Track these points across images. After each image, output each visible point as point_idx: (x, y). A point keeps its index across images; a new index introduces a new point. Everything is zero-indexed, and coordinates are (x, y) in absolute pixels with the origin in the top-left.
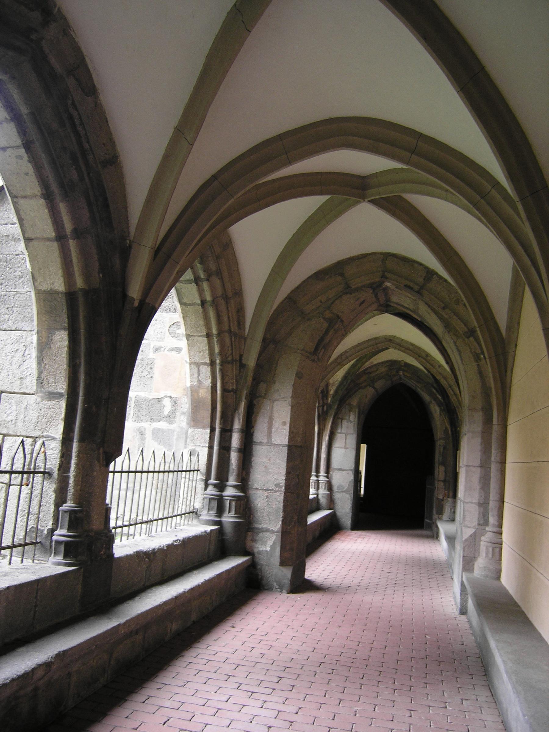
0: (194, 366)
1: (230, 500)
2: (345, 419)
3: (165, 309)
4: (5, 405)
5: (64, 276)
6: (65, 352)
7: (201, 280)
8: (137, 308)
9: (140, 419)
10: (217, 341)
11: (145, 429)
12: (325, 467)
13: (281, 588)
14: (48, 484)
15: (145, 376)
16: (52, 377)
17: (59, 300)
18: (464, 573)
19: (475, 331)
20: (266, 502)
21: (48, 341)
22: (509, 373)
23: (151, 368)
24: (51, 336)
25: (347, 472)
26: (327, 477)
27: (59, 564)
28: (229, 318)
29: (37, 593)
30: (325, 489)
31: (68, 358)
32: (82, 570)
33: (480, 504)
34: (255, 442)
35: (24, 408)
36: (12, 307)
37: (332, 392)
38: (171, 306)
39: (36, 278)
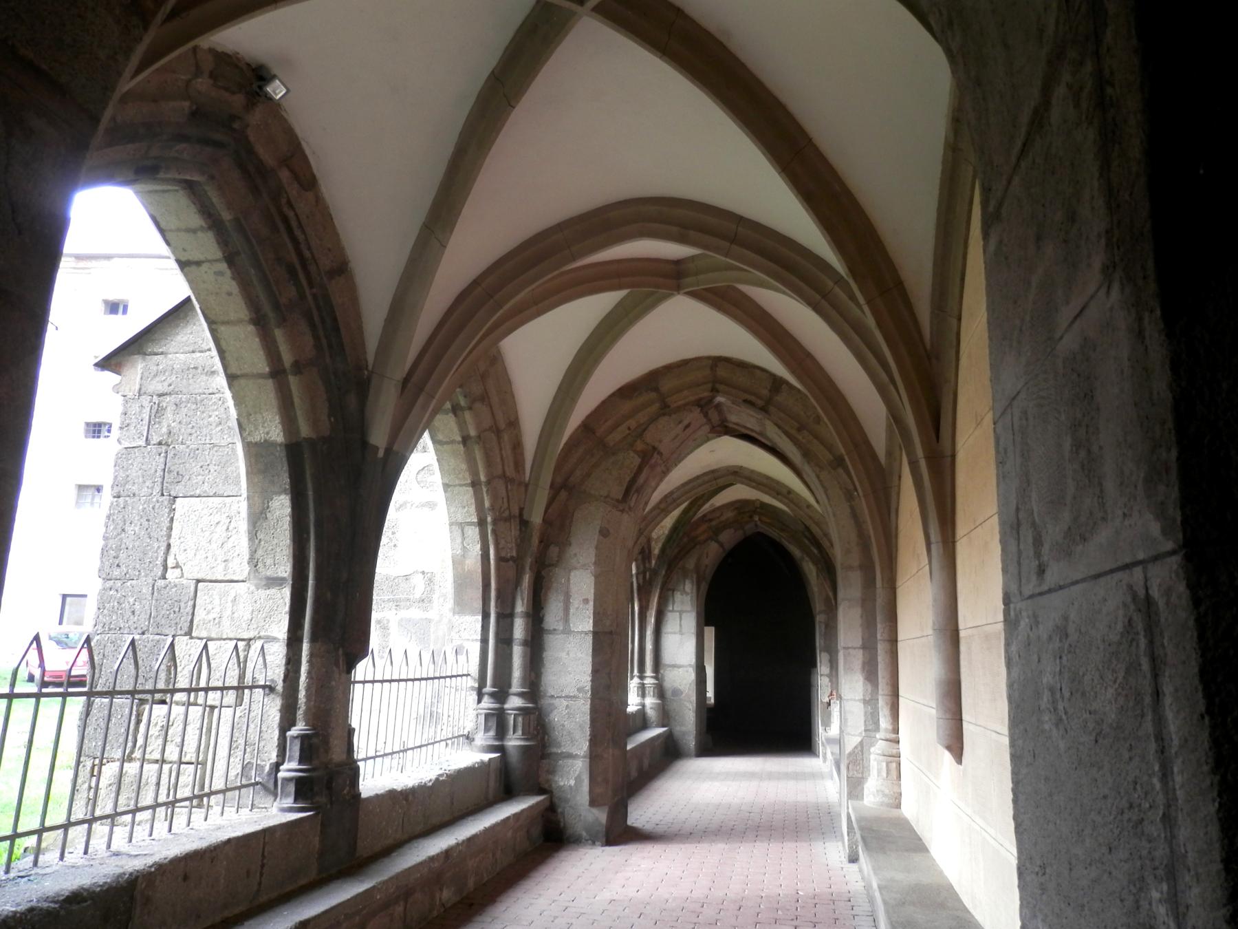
2: (679, 591)
4: (204, 598)
6: (288, 523)
7: (462, 409)
10: (487, 491)
11: (388, 621)
12: (652, 663)
13: (593, 840)
17: (277, 454)
18: (849, 801)
19: (843, 460)
21: (264, 509)
23: (393, 533)
24: (266, 502)
25: (685, 669)
26: (656, 678)
27: (291, 810)
28: (502, 459)
31: (291, 531)
33: (865, 702)
35: (232, 601)
36: (208, 465)
37: (656, 551)
39: (244, 427)
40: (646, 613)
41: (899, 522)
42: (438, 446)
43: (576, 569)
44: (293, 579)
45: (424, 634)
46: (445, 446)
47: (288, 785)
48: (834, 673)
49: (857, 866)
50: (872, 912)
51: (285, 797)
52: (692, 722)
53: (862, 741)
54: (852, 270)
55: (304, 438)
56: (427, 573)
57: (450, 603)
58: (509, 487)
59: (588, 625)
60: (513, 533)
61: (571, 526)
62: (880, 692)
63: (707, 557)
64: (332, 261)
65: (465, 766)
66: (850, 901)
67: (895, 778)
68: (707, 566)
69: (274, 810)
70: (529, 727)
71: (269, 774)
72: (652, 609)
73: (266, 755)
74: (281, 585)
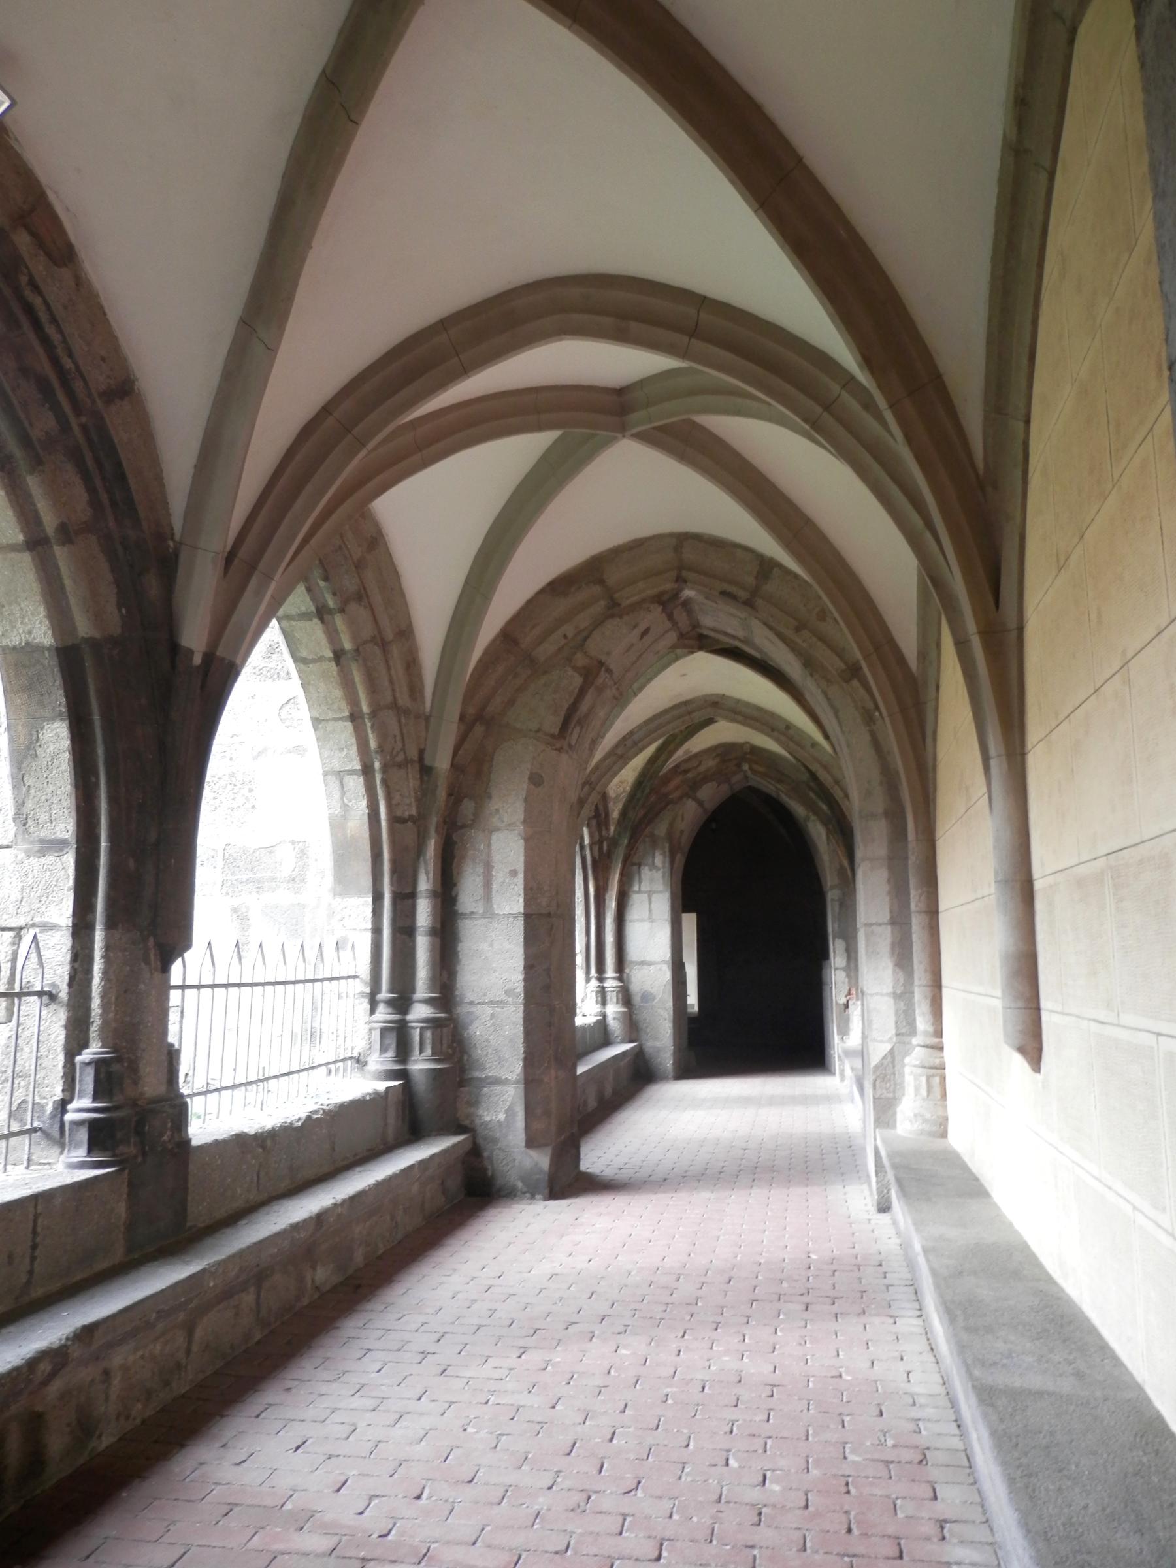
0: (332, 779)
1: (422, 1028)
2: (646, 865)
3: (269, 674)
5: (50, 616)
6: (67, 761)
7: (330, 612)
8: (199, 667)
9: (236, 890)
10: (372, 727)
12: (614, 960)
14: (50, 1015)
15: (239, 807)
16: (44, 810)
18: (877, 1130)
20: (491, 1026)
22: (929, 740)
23: (251, 790)
25: (658, 966)
26: (620, 979)
27: (82, 1165)
28: (391, 682)
29: (35, 1221)
30: (617, 1003)
31: (73, 773)
32: (127, 1171)
33: (897, 996)
34: (462, 914)
37: (615, 814)
38: (279, 668)
40: (604, 895)
41: (938, 750)
42: (302, 666)
43: (498, 829)
44: (78, 841)
45: (296, 925)
46: (311, 666)
47: (77, 1131)
48: (852, 965)
49: (890, 1217)
50: (912, 1280)
51: (75, 1147)
52: (668, 1035)
53: (892, 1049)
54: (868, 361)
55: (83, 638)
56: (299, 842)
57: (329, 880)
58: (403, 721)
59: (517, 905)
60: (411, 785)
61: (490, 773)
62: (916, 982)
63: (683, 820)
64: (109, 377)
65: (351, 1098)
66: (880, 1265)
67: (939, 1097)
68: (682, 832)
69: (60, 1167)
70: (441, 1044)
71: (53, 1116)
72: (612, 890)
73: (48, 1089)
74: (61, 850)
